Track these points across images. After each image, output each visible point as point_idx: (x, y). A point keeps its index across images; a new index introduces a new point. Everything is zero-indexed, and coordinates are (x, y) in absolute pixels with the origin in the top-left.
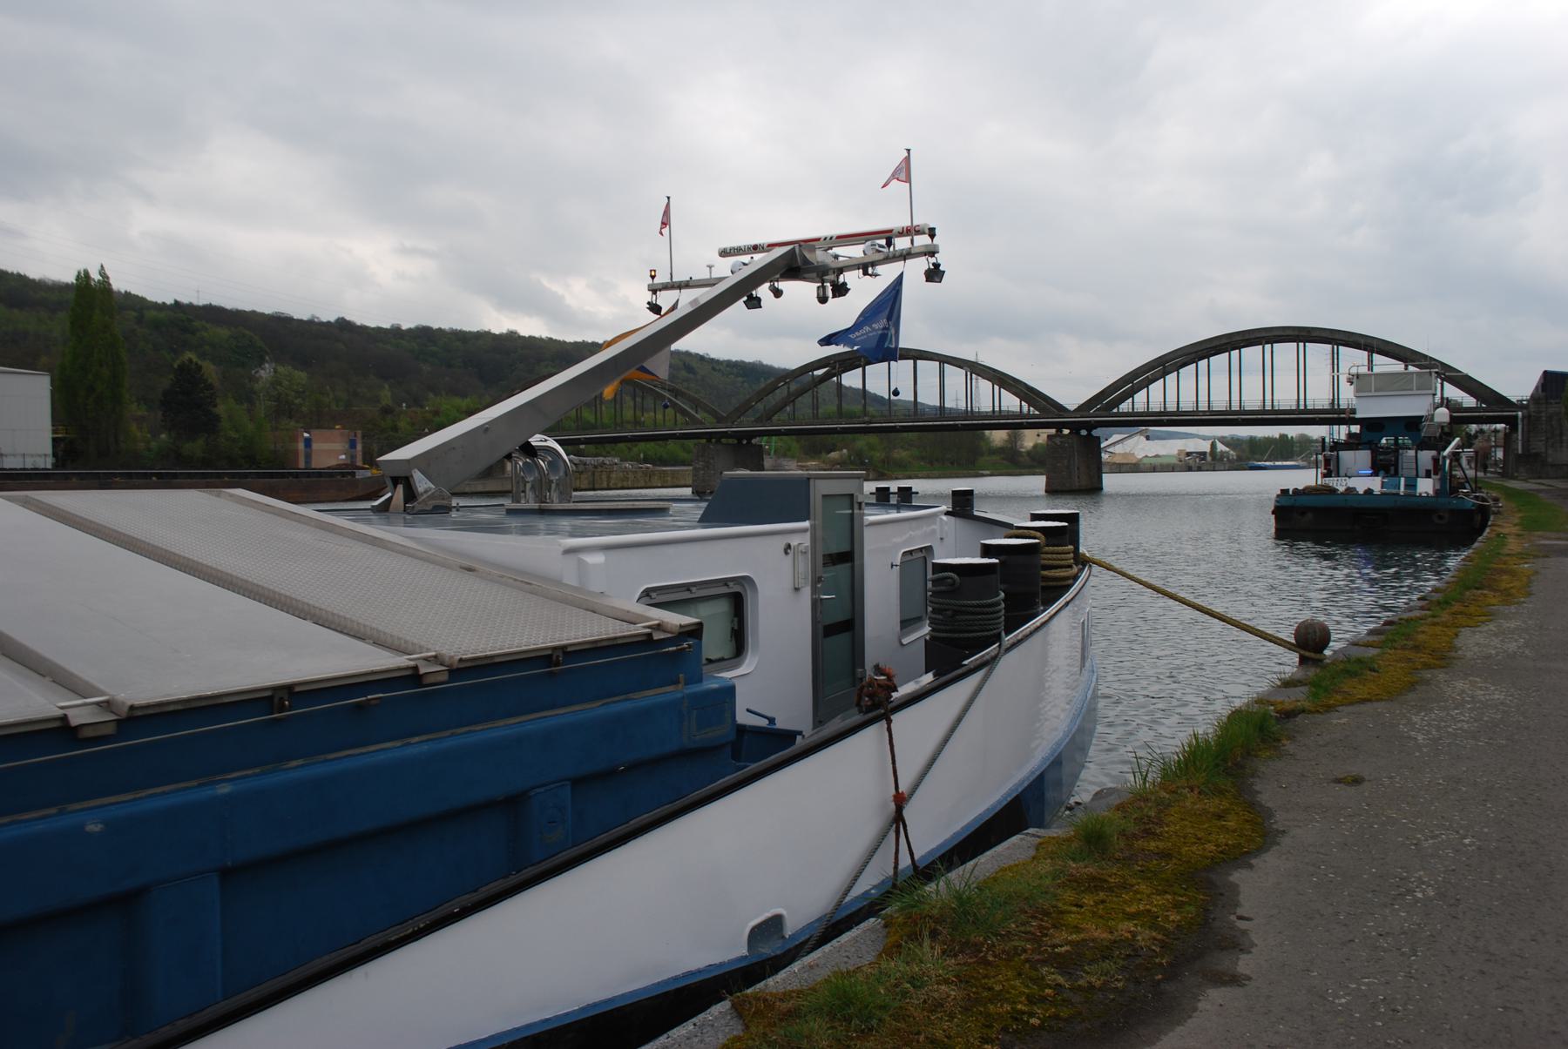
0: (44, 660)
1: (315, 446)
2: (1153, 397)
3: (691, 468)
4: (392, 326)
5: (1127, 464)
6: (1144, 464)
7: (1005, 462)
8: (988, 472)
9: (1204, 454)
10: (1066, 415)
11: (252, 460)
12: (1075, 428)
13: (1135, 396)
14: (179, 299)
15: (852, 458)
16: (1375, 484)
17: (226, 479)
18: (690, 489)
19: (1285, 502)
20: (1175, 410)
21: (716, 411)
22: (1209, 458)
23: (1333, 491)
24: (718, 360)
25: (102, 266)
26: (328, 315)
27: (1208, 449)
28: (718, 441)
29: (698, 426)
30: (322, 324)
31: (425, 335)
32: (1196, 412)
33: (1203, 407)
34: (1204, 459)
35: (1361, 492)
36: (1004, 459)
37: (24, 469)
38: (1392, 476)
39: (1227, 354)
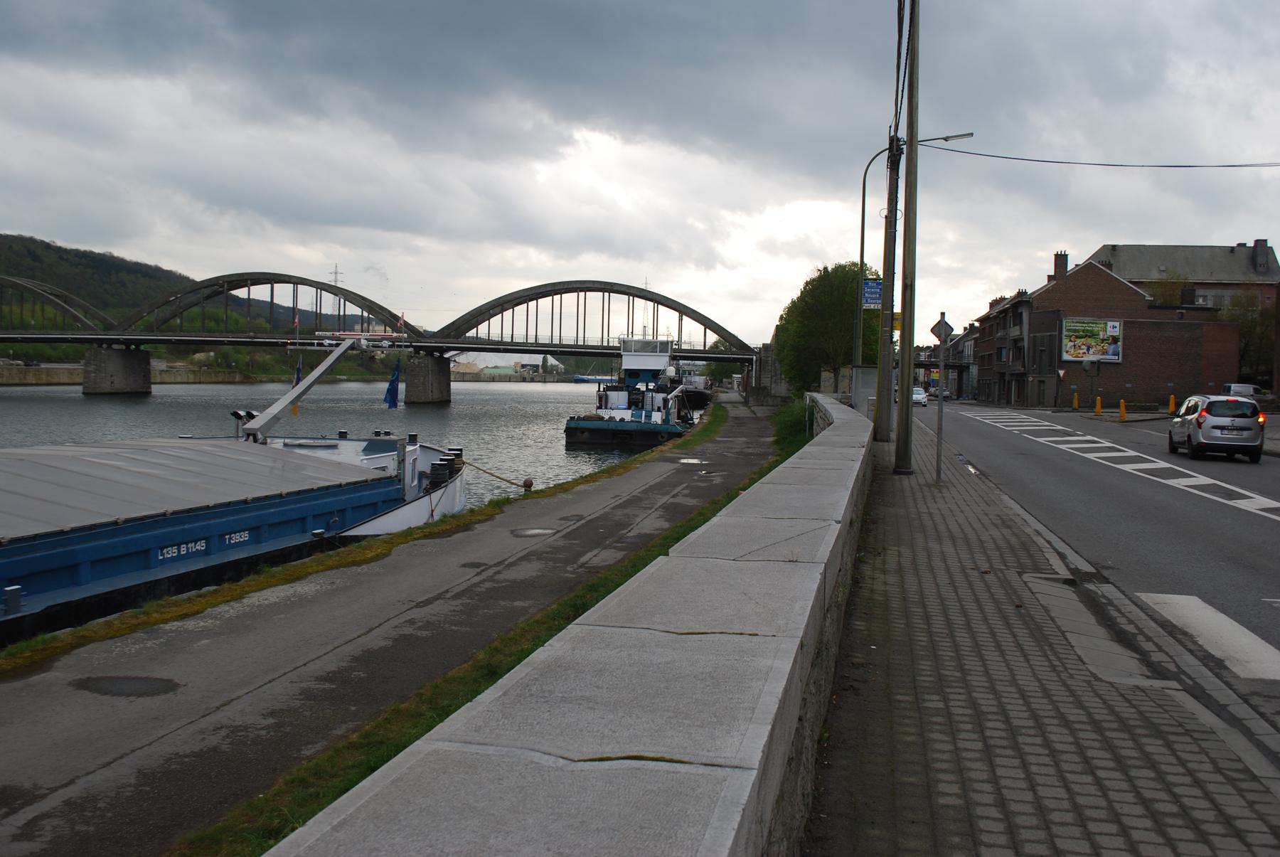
2: (491, 329)
3: (740, 376)
5: (470, 374)
6: (485, 374)
7: (360, 368)
8: (345, 377)
9: (537, 366)
10: (422, 341)
12: (430, 351)
13: (479, 327)
15: (219, 360)
16: (627, 415)
18: (80, 388)
19: (573, 425)
20: (510, 341)
22: (541, 370)
23: (602, 419)
27: (540, 363)
28: (109, 347)
29: (91, 332)
32: (526, 344)
33: (531, 340)
34: (536, 371)
35: (618, 420)
36: (359, 365)
38: (639, 409)
39: (551, 297)
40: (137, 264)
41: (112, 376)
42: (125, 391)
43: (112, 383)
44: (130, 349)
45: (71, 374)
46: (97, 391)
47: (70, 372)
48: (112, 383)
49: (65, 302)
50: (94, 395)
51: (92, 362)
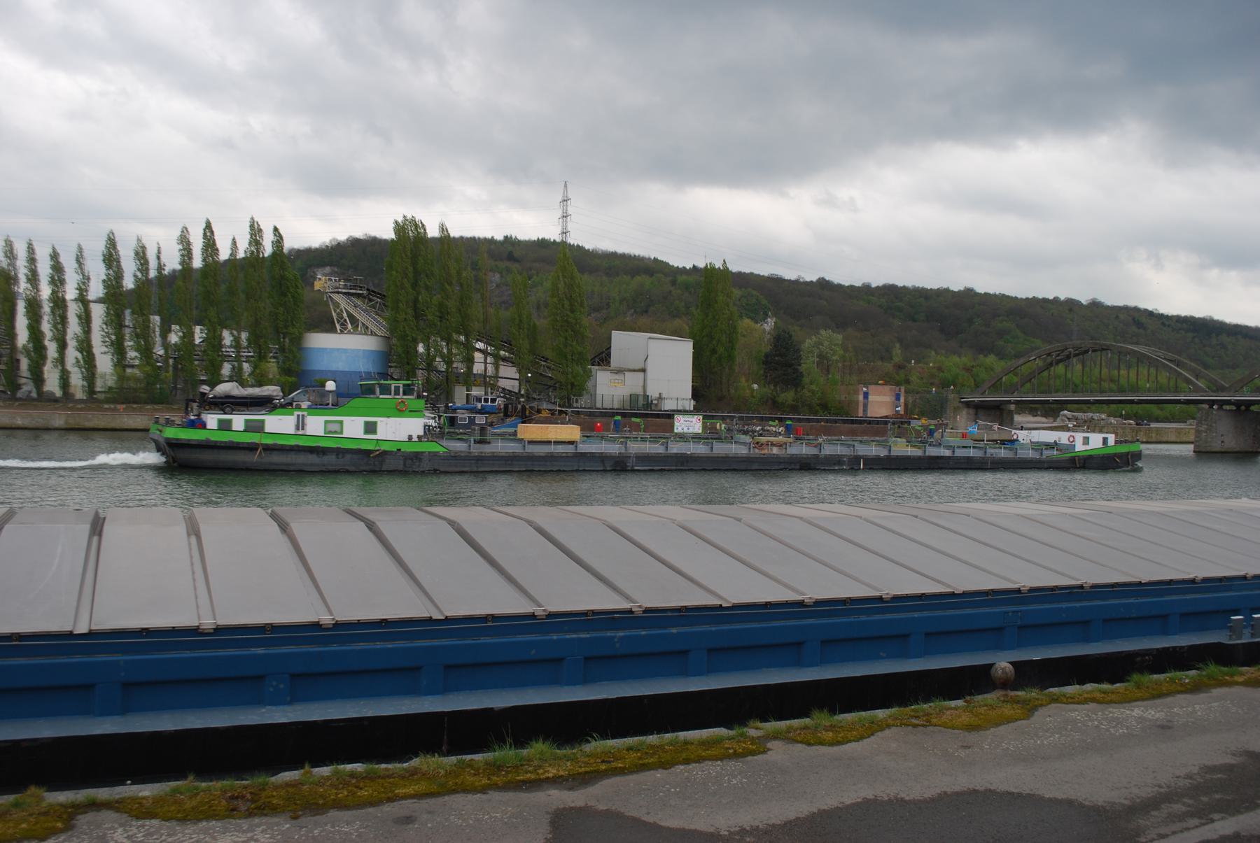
0: (391, 545)
1: (871, 398)
4: (863, 284)
11: (825, 407)
14: (696, 265)
17: (822, 423)
18: (1191, 447)
21: (1216, 381)
24: (1167, 316)
25: (724, 261)
26: (811, 277)
29: (1202, 394)
30: (806, 283)
31: (891, 292)
37: (613, 409)
40: (1237, 326)
41: (1222, 435)
42: (1235, 450)
43: (1222, 442)
44: (1245, 406)
45: (1179, 433)
46: (1208, 449)
47: (1179, 431)
48: (1222, 442)
49: (1177, 366)
50: (1204, 454)
51: (1203, 422)
